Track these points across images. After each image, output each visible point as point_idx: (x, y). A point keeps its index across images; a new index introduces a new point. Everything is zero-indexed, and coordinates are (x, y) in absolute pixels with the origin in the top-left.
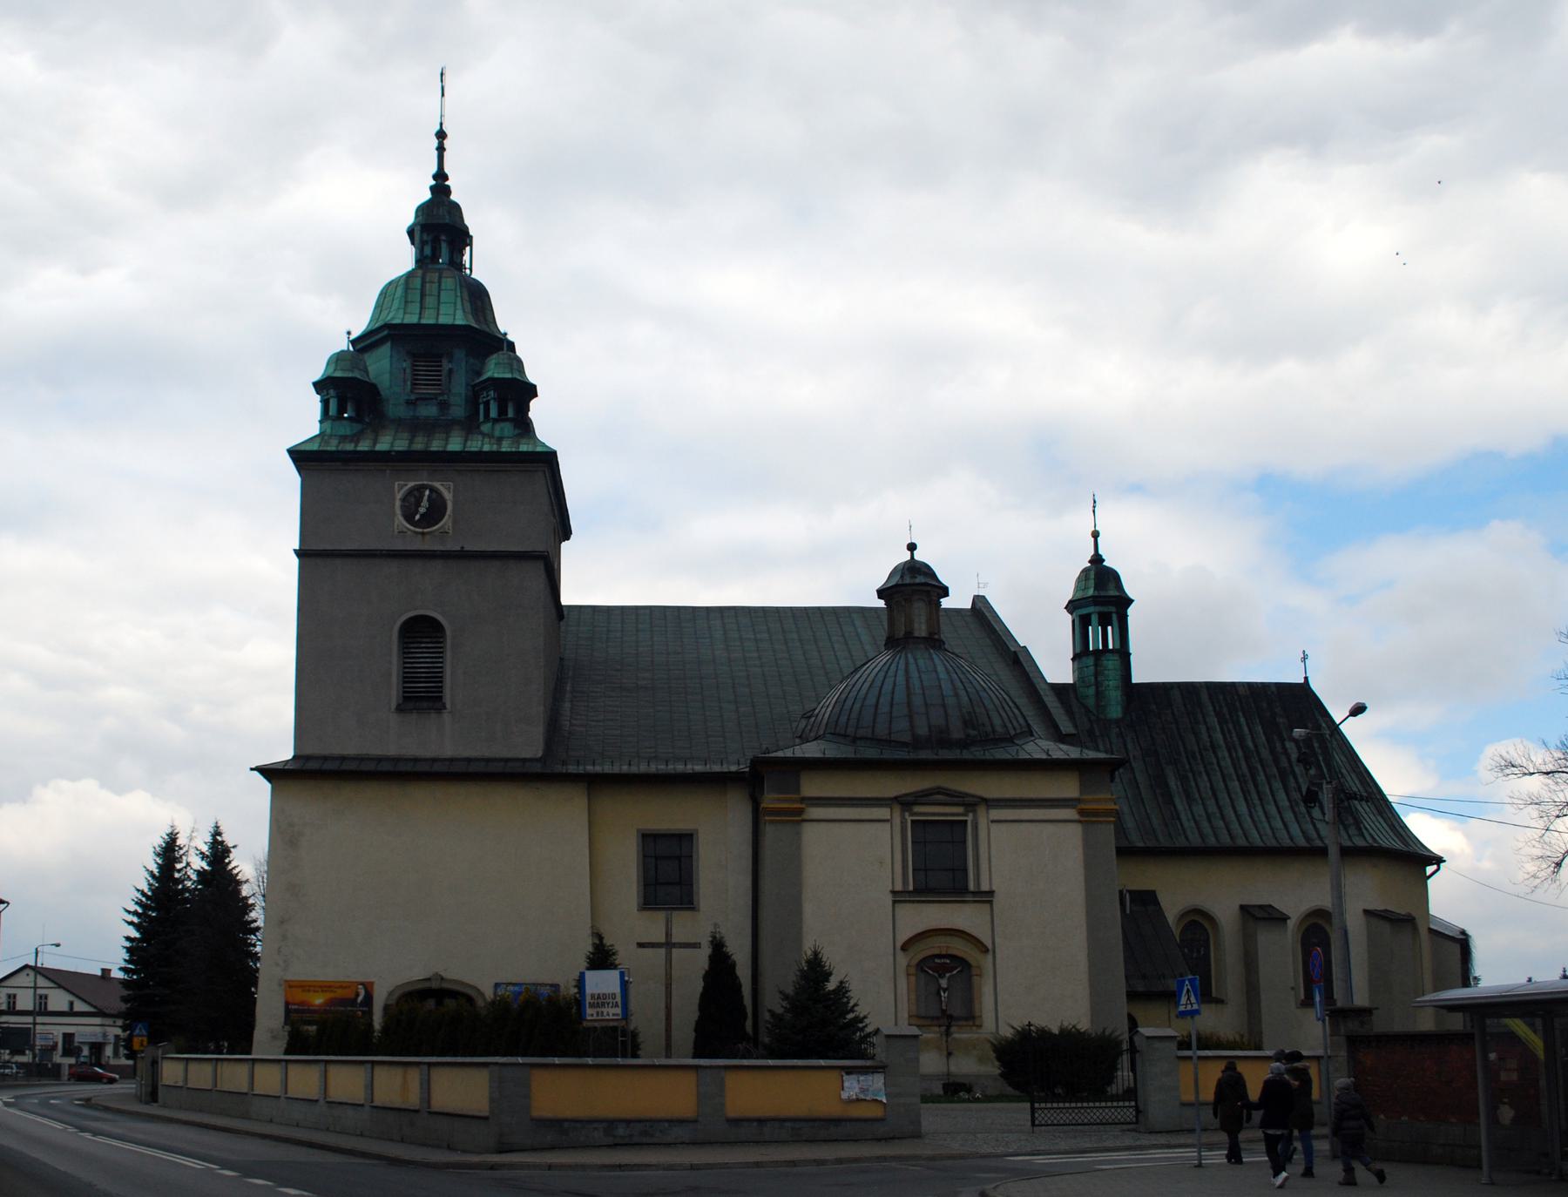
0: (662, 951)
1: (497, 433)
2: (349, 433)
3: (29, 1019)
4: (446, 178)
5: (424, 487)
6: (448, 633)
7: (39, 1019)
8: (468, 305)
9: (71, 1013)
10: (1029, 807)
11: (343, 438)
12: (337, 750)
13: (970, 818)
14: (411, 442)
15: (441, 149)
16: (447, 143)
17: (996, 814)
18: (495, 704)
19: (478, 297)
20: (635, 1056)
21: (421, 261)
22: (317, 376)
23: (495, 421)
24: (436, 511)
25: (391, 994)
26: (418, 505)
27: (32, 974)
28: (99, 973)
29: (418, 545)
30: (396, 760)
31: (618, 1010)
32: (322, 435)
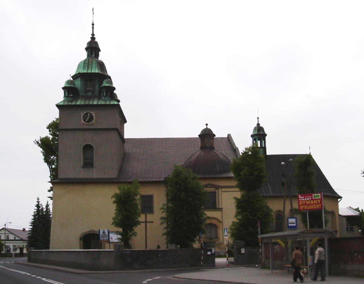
0: (148, 224)
1: (106, 99)
2: (70, 100)
3: (4, 242)
4: (94, 35)
5: (88, 113)
6: (94, 148)
7: (6, 242)
8: (99, 67)
9: (15, 240)
10: (232, 188)
11: (69, 102)
12: (69, 177)
13: (217, 191)
14: (85, 102)
15: (93, 28)
16: (94, 26)
17: (223, 190)
18: (106, 166)
19: (102, 66)
20: (104, 249)
21: (88, 56)
22: (63, 86)
23: (105, 96)
24: (91, 118)
25: (82, 235)
26: (87, 117)
27: (4, 230)
28: (22, 229)
29: (87, 127)
30: (82, 179)
31: (107, 238)
32: (64, 101)
